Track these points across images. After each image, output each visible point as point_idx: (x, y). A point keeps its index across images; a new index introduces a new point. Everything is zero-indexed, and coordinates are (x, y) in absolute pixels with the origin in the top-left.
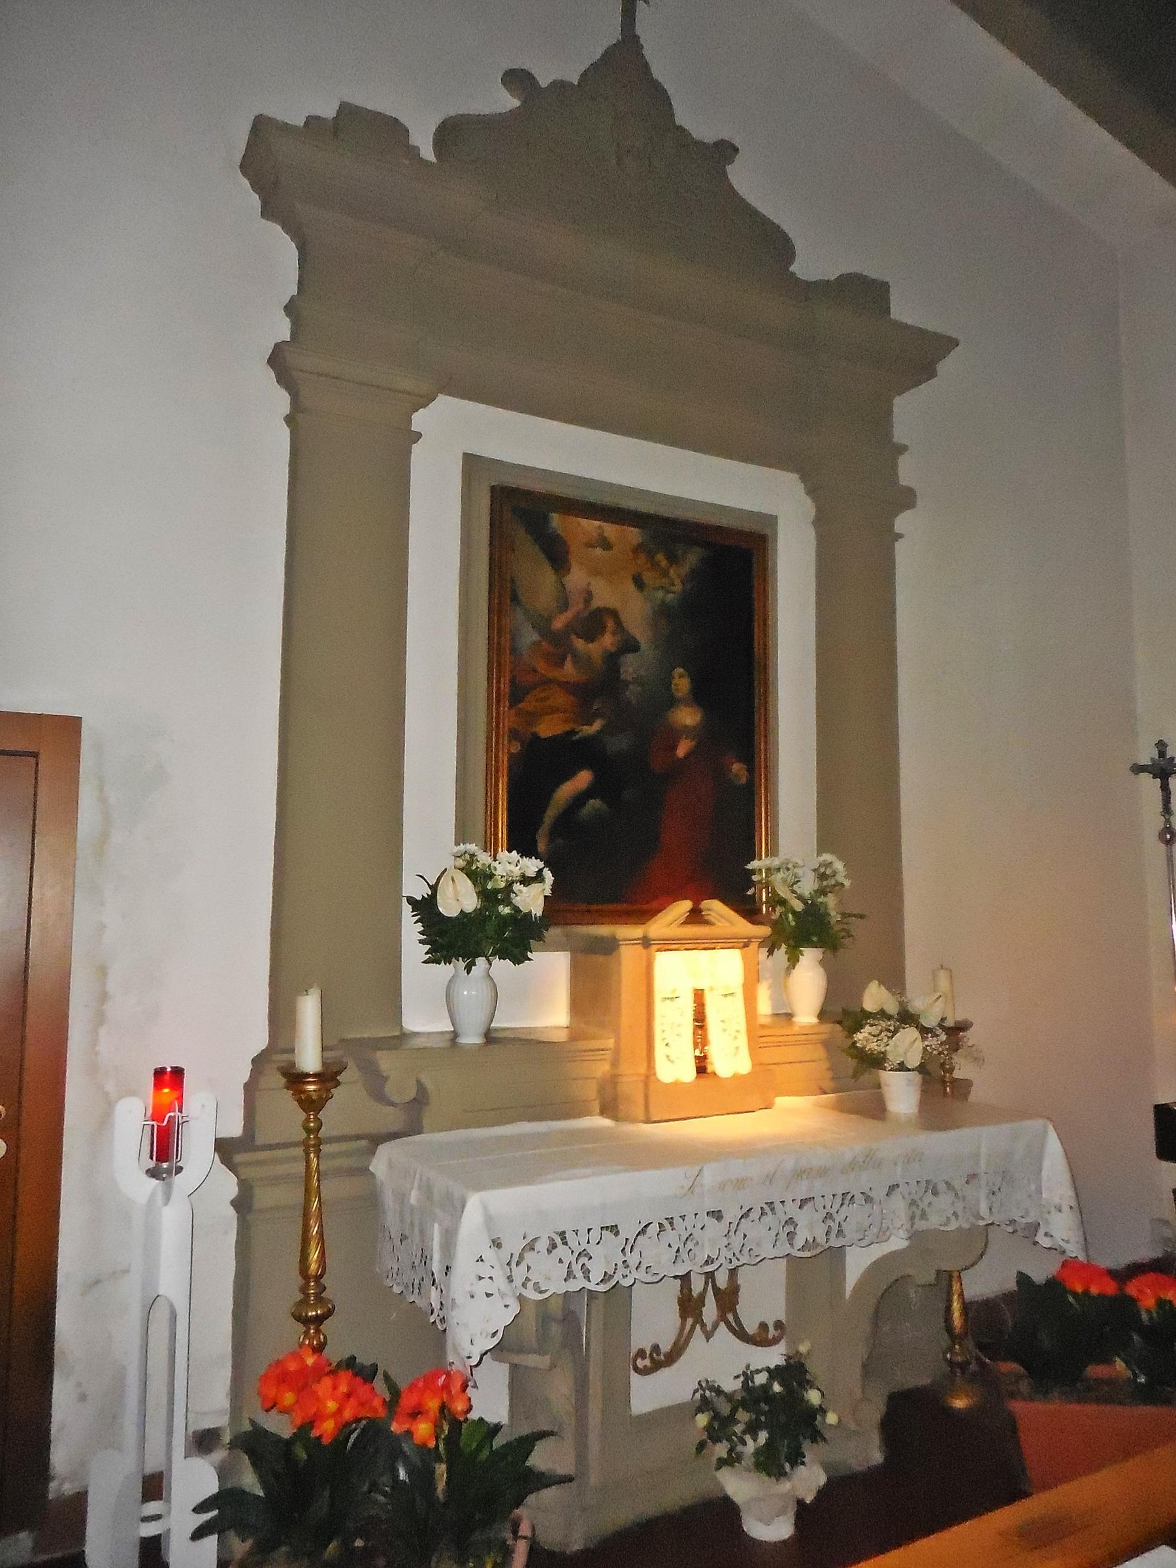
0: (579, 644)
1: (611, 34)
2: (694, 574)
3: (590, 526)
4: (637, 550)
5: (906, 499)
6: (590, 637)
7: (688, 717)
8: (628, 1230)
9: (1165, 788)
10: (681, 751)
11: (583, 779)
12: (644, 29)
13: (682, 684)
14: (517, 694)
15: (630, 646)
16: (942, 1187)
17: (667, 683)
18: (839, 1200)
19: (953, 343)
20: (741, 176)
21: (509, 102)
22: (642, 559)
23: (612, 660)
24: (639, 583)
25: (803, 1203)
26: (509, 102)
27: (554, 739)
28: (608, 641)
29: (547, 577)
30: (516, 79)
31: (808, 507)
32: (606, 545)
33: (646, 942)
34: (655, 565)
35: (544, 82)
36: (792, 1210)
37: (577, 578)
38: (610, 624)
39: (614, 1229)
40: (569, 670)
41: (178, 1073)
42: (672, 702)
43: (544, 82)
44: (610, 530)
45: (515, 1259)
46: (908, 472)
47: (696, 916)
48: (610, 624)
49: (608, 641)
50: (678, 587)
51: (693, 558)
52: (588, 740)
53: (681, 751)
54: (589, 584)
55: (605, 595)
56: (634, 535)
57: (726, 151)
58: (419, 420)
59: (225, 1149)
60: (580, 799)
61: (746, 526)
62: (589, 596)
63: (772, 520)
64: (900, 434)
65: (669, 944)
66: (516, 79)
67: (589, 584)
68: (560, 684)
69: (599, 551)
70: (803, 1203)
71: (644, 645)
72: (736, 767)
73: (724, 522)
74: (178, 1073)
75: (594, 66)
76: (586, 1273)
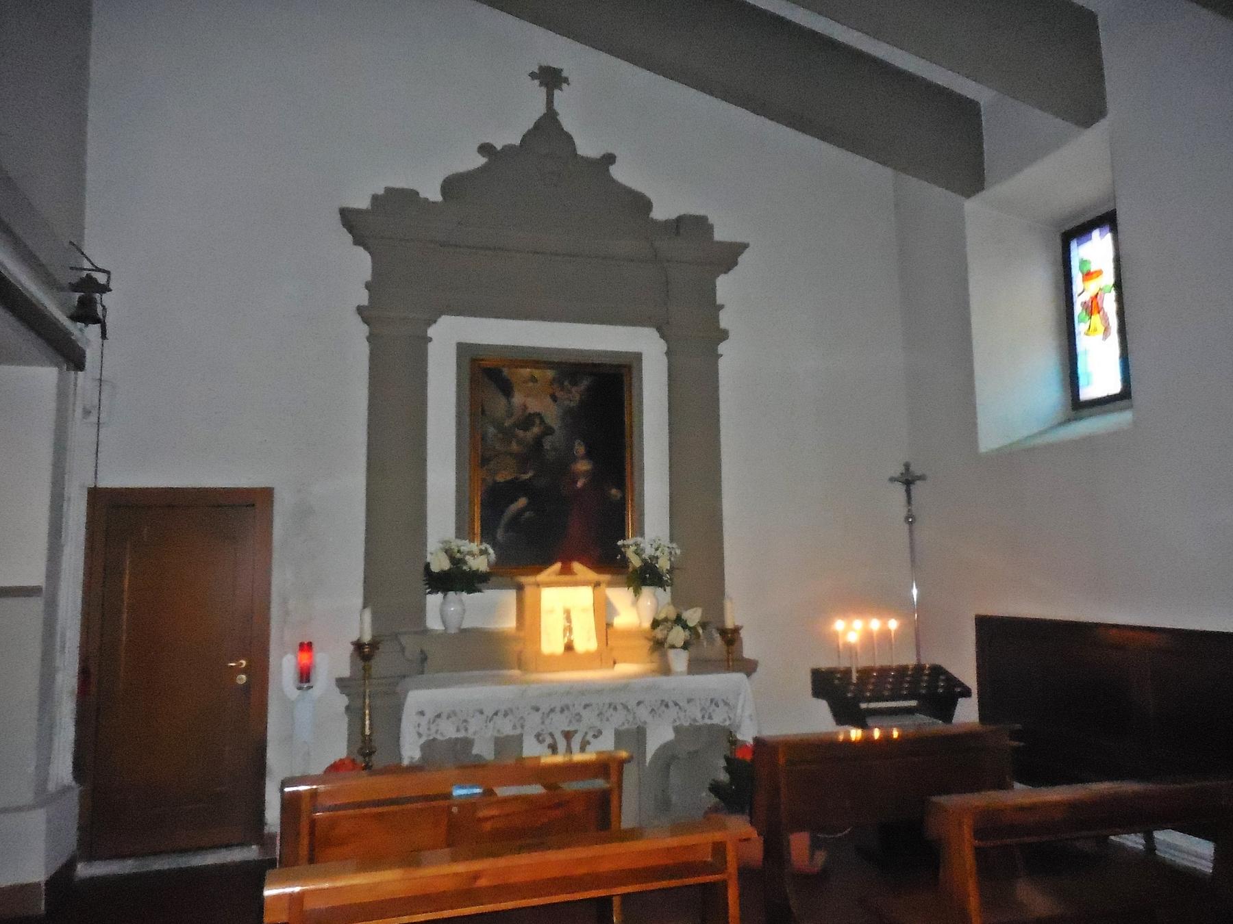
0: (520, 433)
1: (541, 109)
2: (589, 389)
3: (526, 372)
4: (554, 380)
5: (724, 335)
6: (526, 429)
7: (583, 466)
8: (489, 712)
9: (908, 492)
10: (579, 484)
11: (522, 502)
12: (558, 106)
13: (580, 449)
14: (485, 461)
15: (548, 431)
16: (671, 704)
17: (571, 448)
18: (607, 706)
19: (743, 247)
20: (618, 172)
21: (481, 161)
22: (555, 386)
23: (538, 441)
24: (554, 398)
25: (586, 706)
26: (481, 161)
27: (507, 482)
28: (536, 430)
29: (503, 401)
30: (485, 149)
31: (662, 346)
32: (533, 379)
33: (538, 585)
34: (562, 388)
35: (499, 147)
36: (579, 709)
37: (518, 399)
38: (538, 421)
39: (481, 712)
40: (514, 447)
41: (310, 645)
42: (575, 459)
43: (499, 147)
44: (537, 373)
45: (431, 721)
46: (725, 320)
47: (566, 570)
48: (538, 421)
49: (536, 430)
50: (578, 398)
51: (585, 383)
52: (525, 483)
53: (579, 484)
54: (525, 401)
55: (534, 406)
56: (550, 374)
57: (610, 159)
58: (431, 332)
59: (342, 683)
60: (521, 512)
61: (616, 362)
62: (525, 407)
63: (638, 357)
64: (720, 300)
65: (549, 584)
66: (485, 149)
67: (525, 401)
68: (511, 454)
69: (531, 384)
70: (586, 706)
71: (558, 432)
72: (614, 491)
73: (607, 361)
74: (310, 645)
75: (529, 132)
76: (466, 730)
